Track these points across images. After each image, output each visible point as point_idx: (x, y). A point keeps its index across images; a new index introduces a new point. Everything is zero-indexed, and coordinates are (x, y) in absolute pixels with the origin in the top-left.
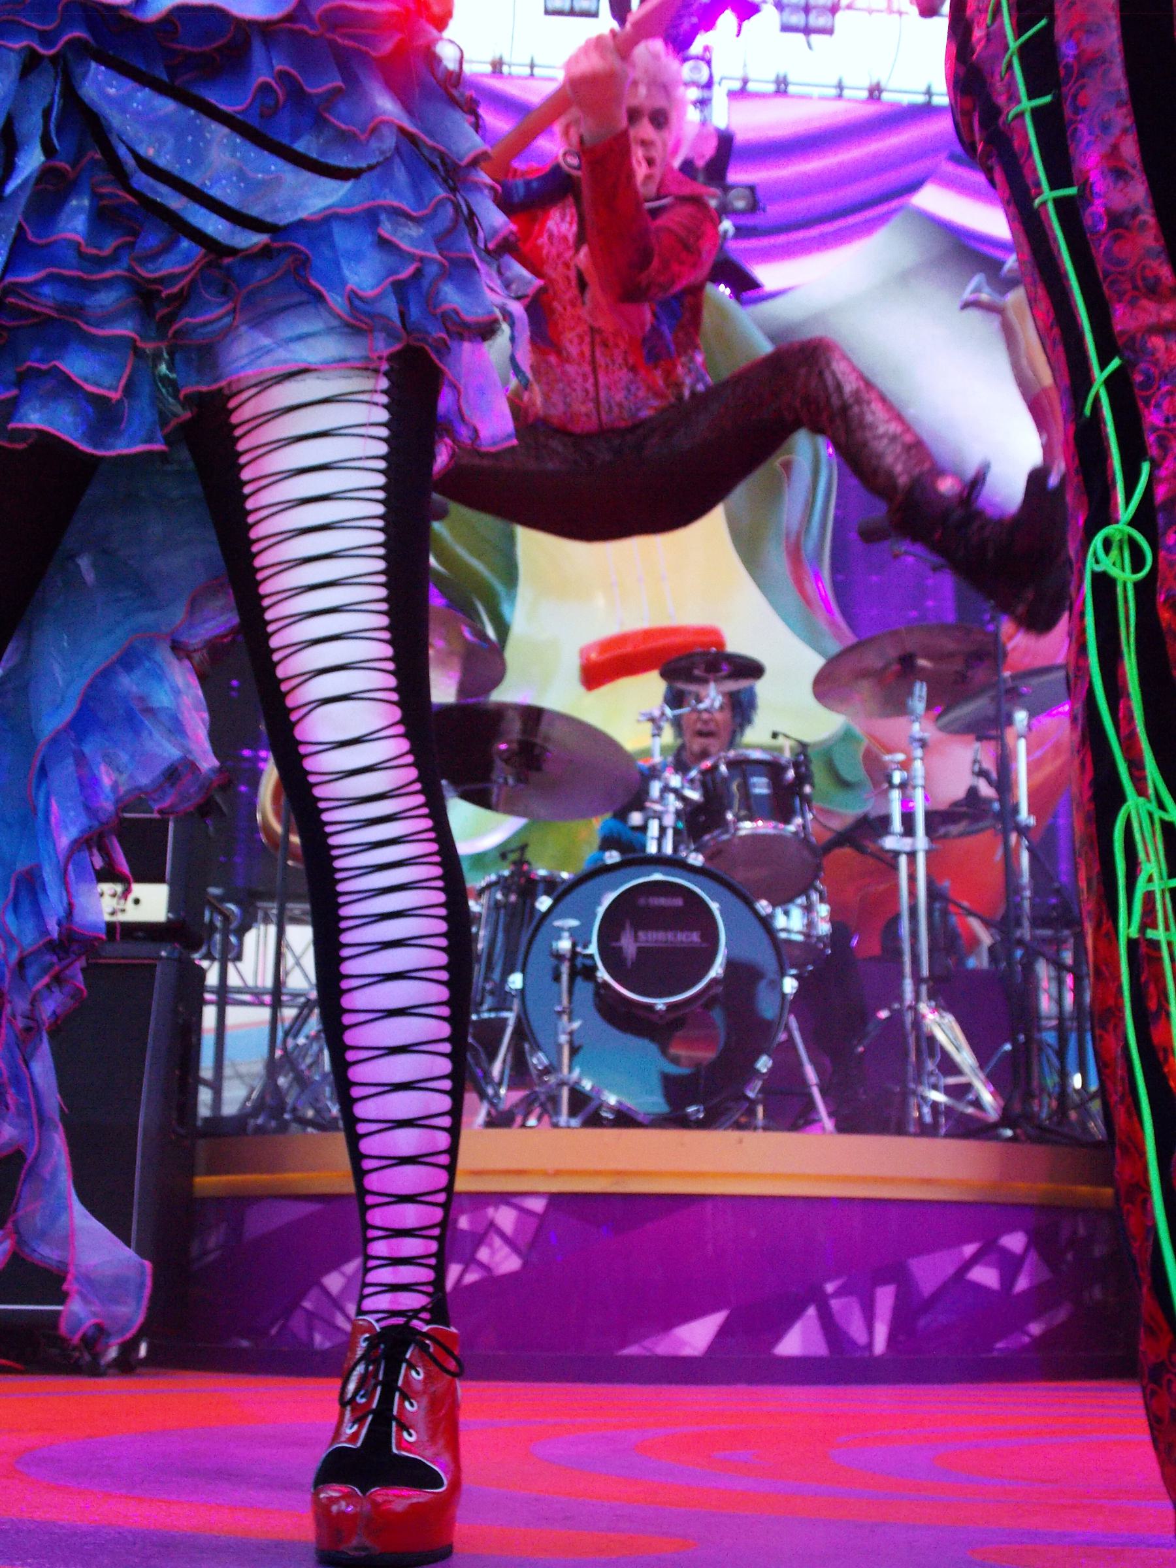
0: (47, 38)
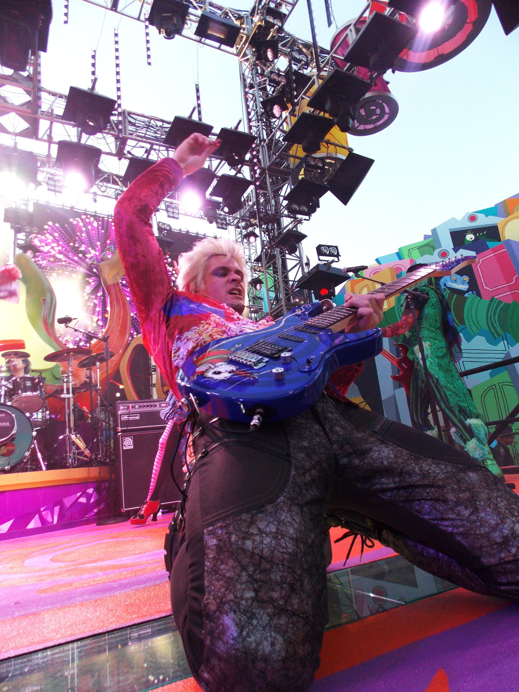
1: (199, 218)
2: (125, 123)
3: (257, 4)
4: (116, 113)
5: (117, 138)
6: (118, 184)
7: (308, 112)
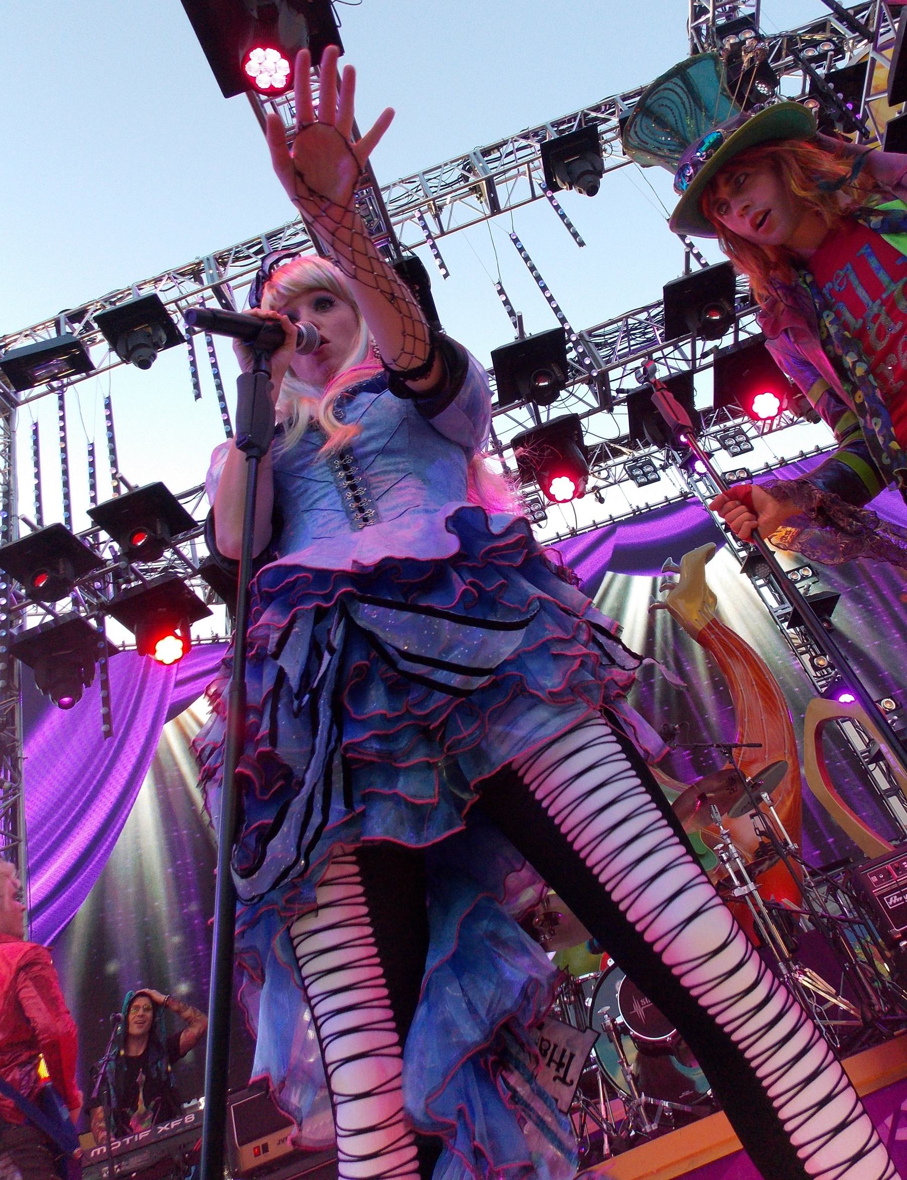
0: (327, 597)
1: (788, 426)
2: (590, 350)
3: (696, 41)
4: (571, 345)
5: (589, 381)
6: (623, 453)
7: (897, 115)
